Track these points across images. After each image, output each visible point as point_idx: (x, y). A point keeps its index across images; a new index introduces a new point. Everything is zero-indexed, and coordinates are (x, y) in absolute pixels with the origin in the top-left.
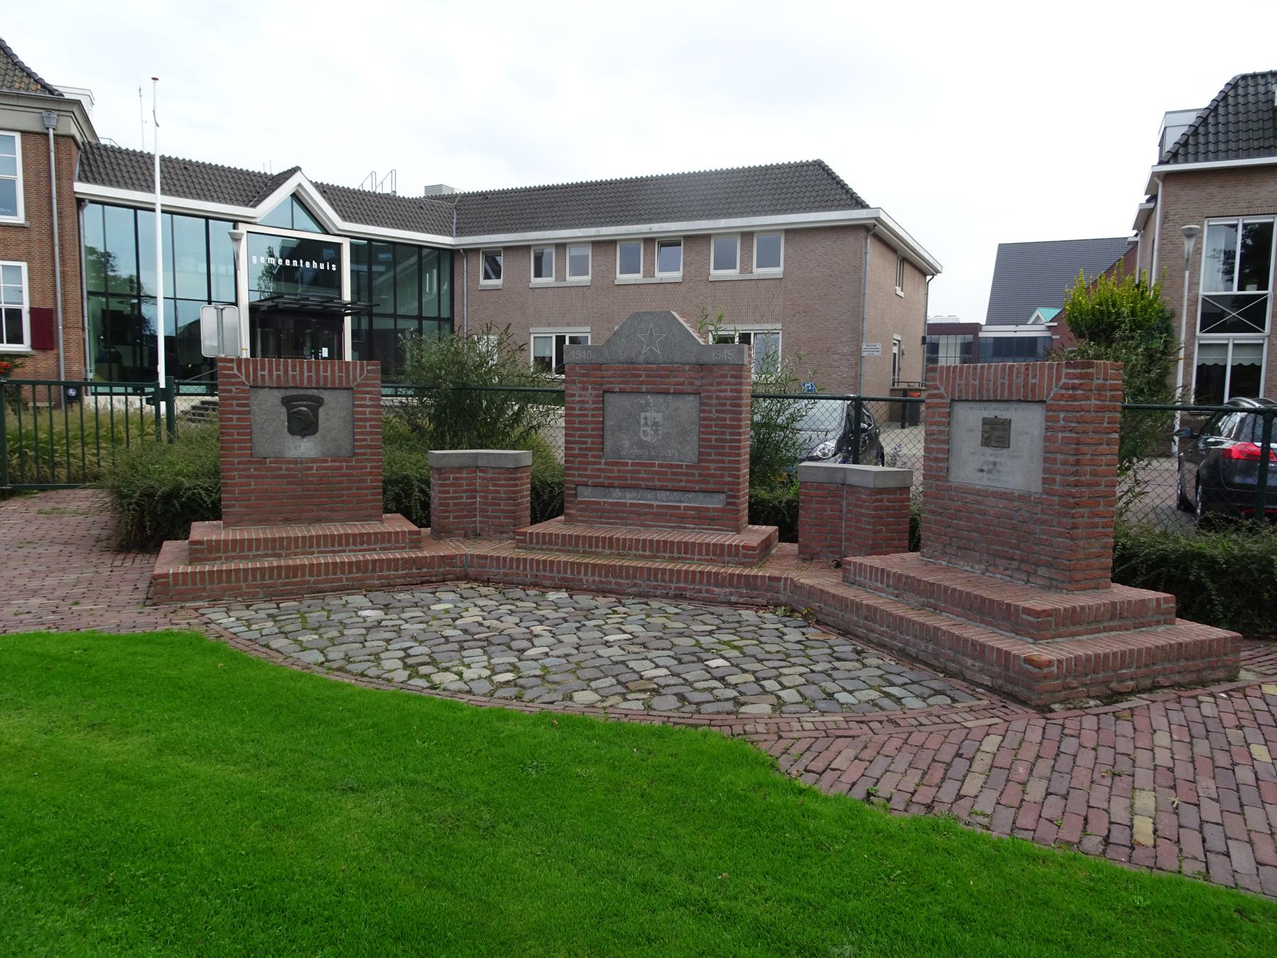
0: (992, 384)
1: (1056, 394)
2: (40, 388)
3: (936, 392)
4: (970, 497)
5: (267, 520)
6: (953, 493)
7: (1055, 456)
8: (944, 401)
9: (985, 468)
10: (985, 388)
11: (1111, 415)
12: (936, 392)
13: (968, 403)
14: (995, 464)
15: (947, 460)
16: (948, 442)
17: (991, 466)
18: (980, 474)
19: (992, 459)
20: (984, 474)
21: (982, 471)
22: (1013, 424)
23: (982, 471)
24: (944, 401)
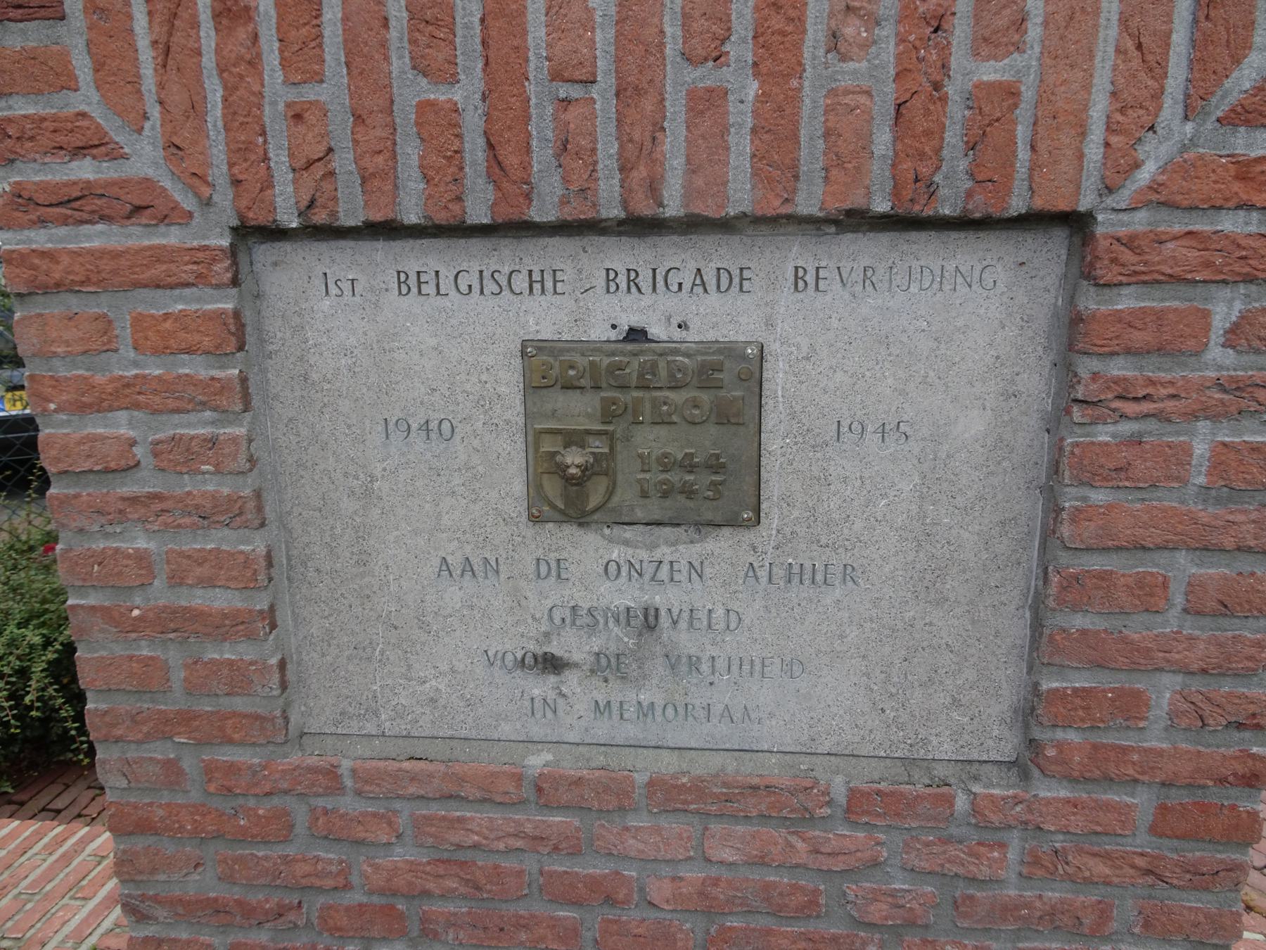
0: (602, 95)
1: (1180, 167)
2: (821, 275)
3: (85, 170)
4: (478, 816)
5: (157, 444)
6: (348, 804)
7: (1152, 566)
8: (172, 237)
9: (570, 645)
10: (542, 127)
11: (399, 63)
12: (85, 170)
13: (380, 251)
14: (649, 621)
15: (270, 618)
16: (726, 416)
17: (617, 637)
18: (540, 687)
19: (625, 596)
20: (571, 680)
21: (551, 664)
22: (777, 378)
23: (551, 664)
24: (172, 237)
